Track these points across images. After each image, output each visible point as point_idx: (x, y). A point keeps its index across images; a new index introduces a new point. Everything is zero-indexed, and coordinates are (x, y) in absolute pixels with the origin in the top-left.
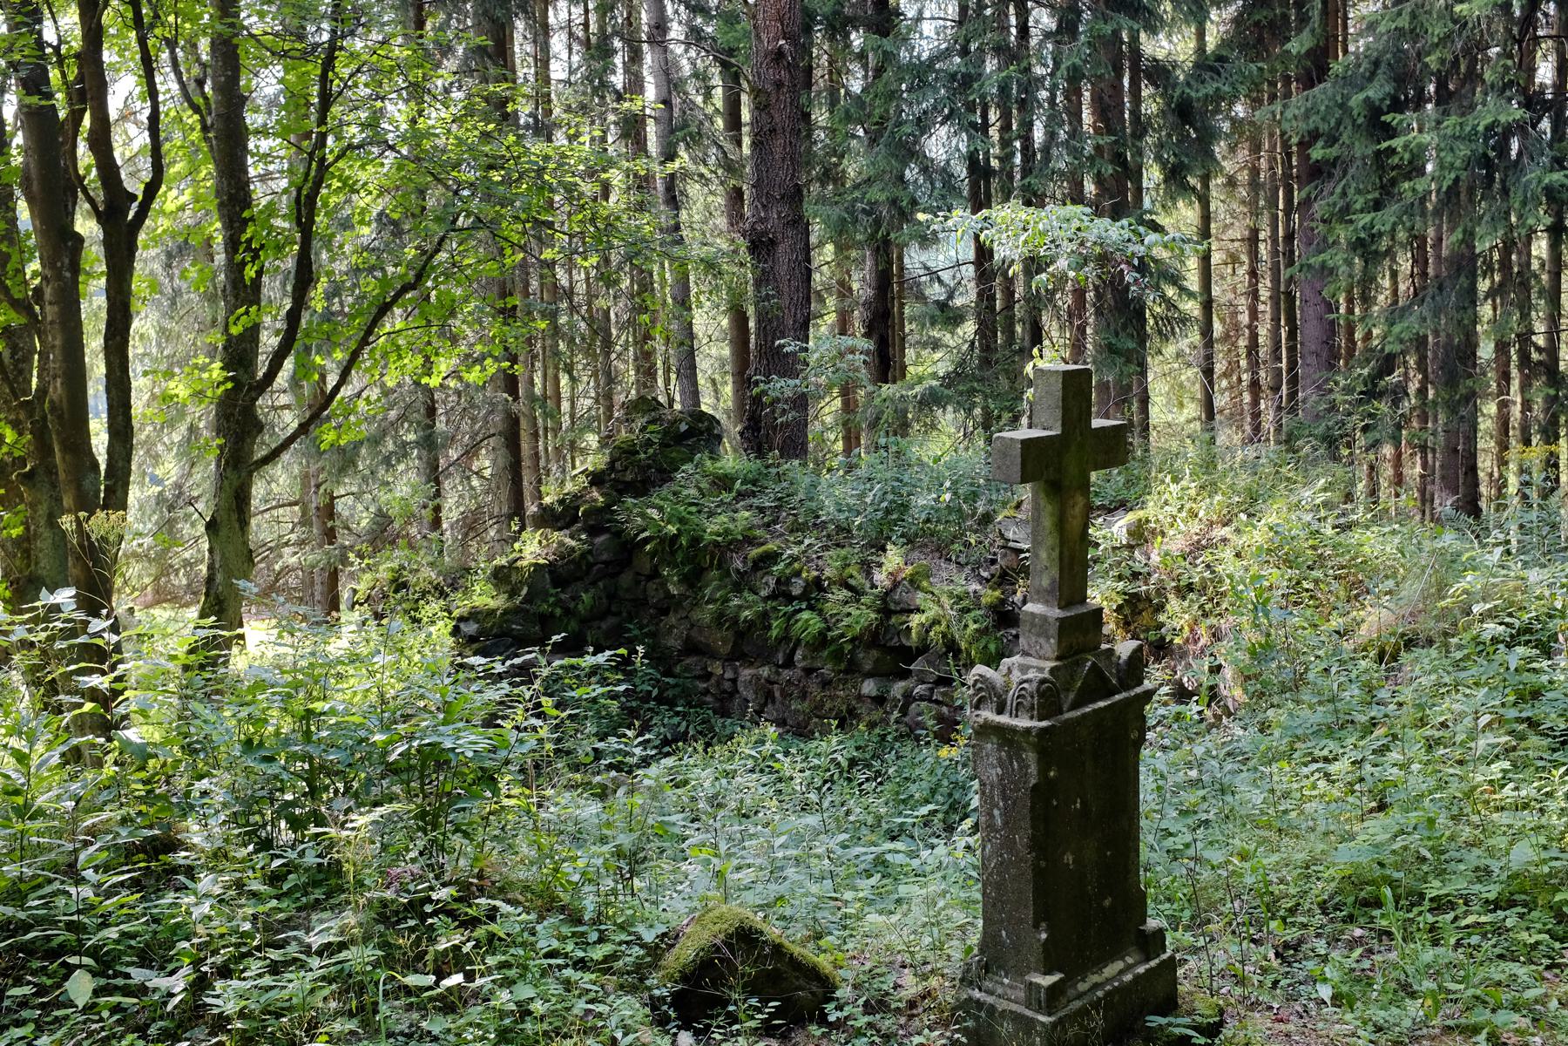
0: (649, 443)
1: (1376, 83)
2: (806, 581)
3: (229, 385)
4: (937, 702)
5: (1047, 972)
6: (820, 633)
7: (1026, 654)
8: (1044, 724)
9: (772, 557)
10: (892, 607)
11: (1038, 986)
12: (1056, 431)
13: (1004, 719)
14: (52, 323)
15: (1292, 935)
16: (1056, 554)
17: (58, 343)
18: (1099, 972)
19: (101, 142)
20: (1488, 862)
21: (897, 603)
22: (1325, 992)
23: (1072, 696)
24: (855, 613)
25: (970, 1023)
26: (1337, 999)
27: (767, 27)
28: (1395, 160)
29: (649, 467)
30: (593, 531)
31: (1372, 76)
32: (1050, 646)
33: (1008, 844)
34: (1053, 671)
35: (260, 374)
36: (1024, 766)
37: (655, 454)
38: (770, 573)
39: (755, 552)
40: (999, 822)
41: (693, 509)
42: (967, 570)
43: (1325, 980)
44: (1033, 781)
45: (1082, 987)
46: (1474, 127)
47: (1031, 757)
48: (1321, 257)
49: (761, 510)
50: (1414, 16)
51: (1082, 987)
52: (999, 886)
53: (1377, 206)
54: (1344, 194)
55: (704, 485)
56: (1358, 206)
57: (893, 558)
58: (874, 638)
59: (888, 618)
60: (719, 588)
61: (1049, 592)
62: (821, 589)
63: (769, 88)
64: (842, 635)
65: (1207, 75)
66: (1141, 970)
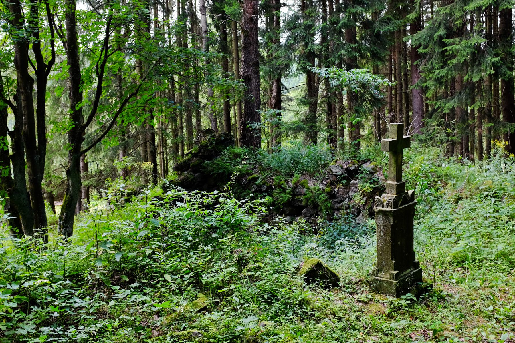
0: (211, 144)
1: (440, 29)
2: (267, 186)
3: (74, 126)
4: (310, 223)
5: (395, 271)
6: (272, 202)
7: (387, 193)
8: (395, 209)
9: (256, 179)
10: (296, 193)
11: (393, 274)
12: (396, 139)
13: (384, 209)
14: (24, 107)
15: (443, 270)
16: (395, 169)
17: (26, 113)
18: (405, 271)
19: (37, 48)
20: (491, 250)
21: (297, 192)
22: (454, 281)
23: (400, 203)
24: (284, 196)
25: (375, 285)
26: (458, 282)
27: (247, 10)
28: (447, 53)
29: (212, 151)
30: (195, 172)
31: (439, 27)
32: (394, 191)
33: (385, 240)
34: (395, 197)
35: (85, 123)
36: (389, 220)
37: (214, 147)
38: (255, 184)
39: (250, 177)
40: (382, 234)
41: (228, 164)
42: (320, 182)
43: (454, 278)
44: (392, 223)
45: (402, 275)
46: (471, 44)
47: (391, 218)
48: (425, 84)
49: (250, 164)
50: (451, 9)
51: (402, 275)
52: (382, 250)
53: (442, 67)
54: (432, 64)
55: (231, 157)
56: (436, 68)
57: (297, 176)
58: (290, 203)
59: (295, 197)
60: (238, 189)
61: (394, 178)
62: (273, 189)
63: (248, 30)
64: (280, 203)
65: (385, 24)
66: (415, 271)
